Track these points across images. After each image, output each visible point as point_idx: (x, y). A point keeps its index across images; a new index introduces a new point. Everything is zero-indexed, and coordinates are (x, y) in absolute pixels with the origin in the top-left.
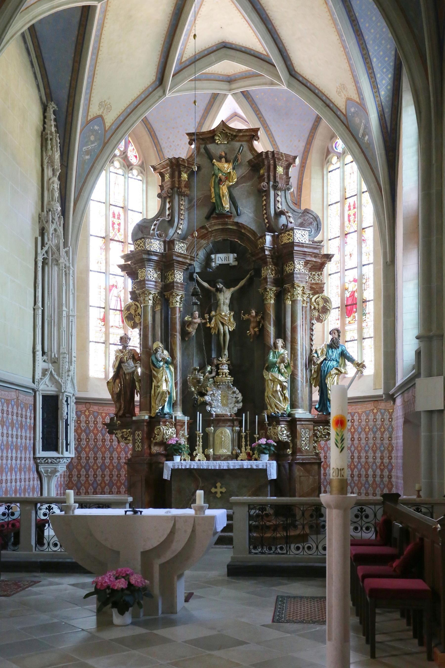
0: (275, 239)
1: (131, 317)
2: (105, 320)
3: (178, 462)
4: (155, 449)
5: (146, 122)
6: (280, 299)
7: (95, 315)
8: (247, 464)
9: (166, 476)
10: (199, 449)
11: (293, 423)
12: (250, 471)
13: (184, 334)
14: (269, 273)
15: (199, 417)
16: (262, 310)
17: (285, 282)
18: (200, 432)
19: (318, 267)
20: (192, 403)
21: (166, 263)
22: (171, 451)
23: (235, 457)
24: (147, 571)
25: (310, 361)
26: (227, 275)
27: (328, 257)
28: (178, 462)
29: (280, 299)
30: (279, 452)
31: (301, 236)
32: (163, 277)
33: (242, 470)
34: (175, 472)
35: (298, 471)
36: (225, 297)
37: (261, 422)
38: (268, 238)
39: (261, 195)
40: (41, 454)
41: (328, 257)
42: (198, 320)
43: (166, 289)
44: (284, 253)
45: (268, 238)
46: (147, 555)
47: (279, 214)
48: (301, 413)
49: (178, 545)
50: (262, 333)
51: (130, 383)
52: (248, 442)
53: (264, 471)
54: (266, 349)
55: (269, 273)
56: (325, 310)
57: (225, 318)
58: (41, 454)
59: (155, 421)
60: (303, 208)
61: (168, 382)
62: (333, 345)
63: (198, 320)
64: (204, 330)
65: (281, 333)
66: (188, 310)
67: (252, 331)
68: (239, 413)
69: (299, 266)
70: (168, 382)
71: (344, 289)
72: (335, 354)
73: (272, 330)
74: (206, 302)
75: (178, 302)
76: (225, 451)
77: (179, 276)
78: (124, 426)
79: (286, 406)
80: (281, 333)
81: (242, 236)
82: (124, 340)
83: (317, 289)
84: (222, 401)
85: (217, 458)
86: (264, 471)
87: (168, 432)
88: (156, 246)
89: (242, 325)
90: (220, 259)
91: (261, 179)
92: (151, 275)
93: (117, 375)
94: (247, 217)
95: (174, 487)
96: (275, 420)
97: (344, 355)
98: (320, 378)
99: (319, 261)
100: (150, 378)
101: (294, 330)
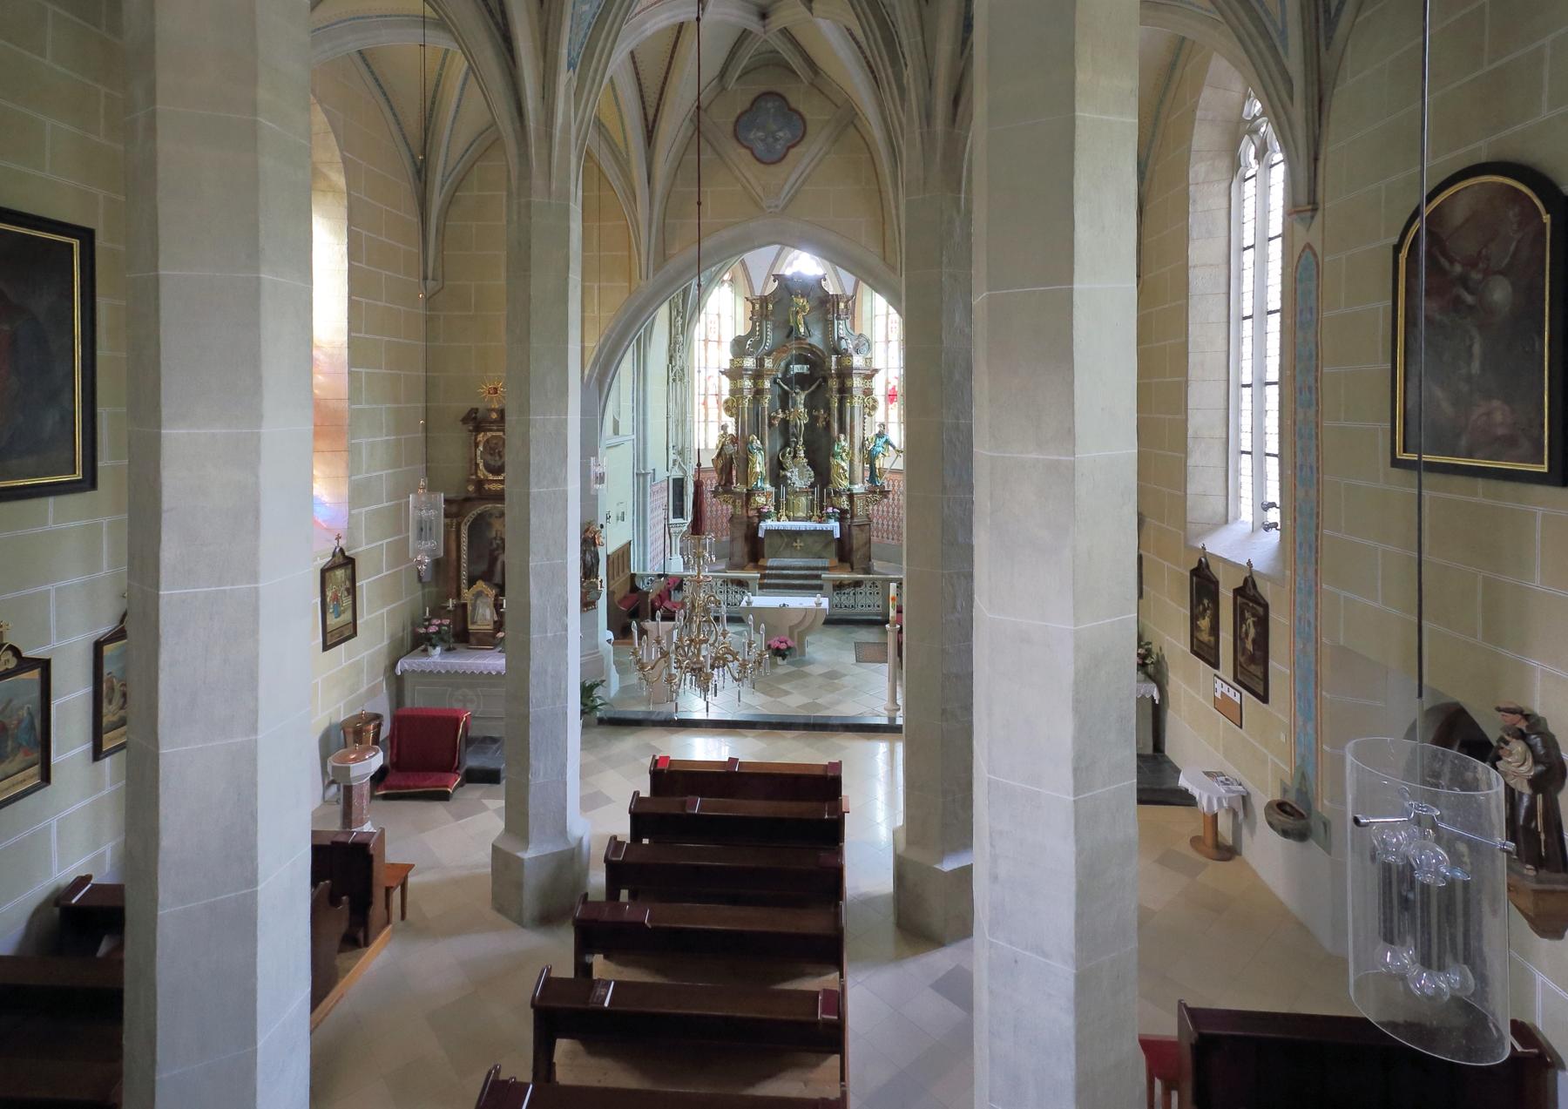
0: (839, 362)
1: (731, 407)
2: (705, 403)
3: (770, 524)
4: (751, 513)
5: (743, 263)
6: (842, 402)
7: (699, 400)
8: (819, 526)
9: (761, 534)
10: (783, 512)
11: (851, 497)
12: (822, 532)
13: (771, 425)
14: (834, 384)
15: (783, 489)
16: (828, 409)
17: (845, 391)
18: (783, 500)
19: (869, 377)
20: (777, 473)
21: (758, 375)
22: (763, 516)
23: (809, 519)
24: (791, 636)
25: (863, 445)
26: (802, 381)
27: (876, 371)
28: (770, 524)
29: (842, 402)
30: (842, 516)
31: (857, 361)
32: (755, 384)
33: (815, 531)
34: (768, 532)
35: (855, 531)
36: (801, 398)
37: (829, 494)
38: (834, 358)
39: (828, 327)
40: (672, 521)
41: (876, 371)
42: (781, 415)
43: (758, 393)
44: (845, 374)
45: (834, 358)
46: (791, 629)
47: (840, 339)
48: (858, 488)
49: (807, 623)
50: (828, 426)
51: (731, 462)
52: (819, 508)
53: (831, 532)
54: (832, 441)
55: (834, 384)
56: (874, 408)
57: (800, 413)
58: (672, 521)
59: (750, 494)
60: (857, 332)
61: (760, 465)
62: (880, 435)
63: (781, 415)
64: (785, 422)
65: (842, 430)
66: (772, 408)
67: (821, 424)
68: (812, 486)
69: (857, 382)
70: (760, 465)
71: (888, 383)
72: (880, 442)
73: (836, 426)
74: (785, 401)
75: (766, 403)
76: (801, 514)
77: (767, 384)
78: (726, 492)
79: (845, 483)
80: (842, 430)
81: (813, 353)
82: (724, 428)
83: (868, 392)
84: (799, 476)
85: (795, 519)
86: (831, 532)
87: (761, 500)
88: (749, 363)
89: (813, 420)
90: (797, 369)
91: (827, 312)
92: (748, 383)
93: (719, 455)
94: (816, 339)
95: (767, 542)
96: (838, 493)
97: (887, 442)
98: (871, 458)
99: (869, 376)
100: (747, 462)
101: (852, 428)
